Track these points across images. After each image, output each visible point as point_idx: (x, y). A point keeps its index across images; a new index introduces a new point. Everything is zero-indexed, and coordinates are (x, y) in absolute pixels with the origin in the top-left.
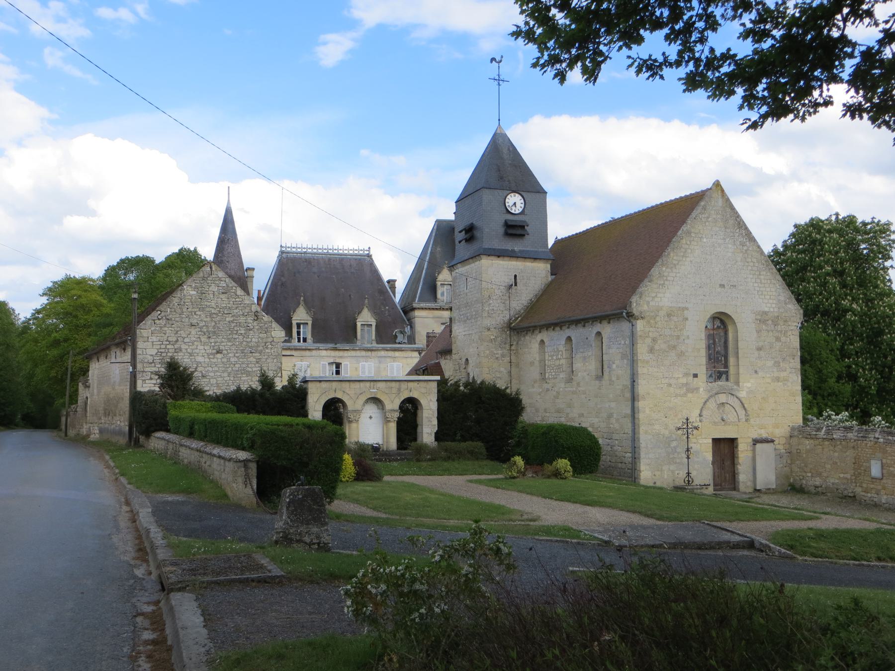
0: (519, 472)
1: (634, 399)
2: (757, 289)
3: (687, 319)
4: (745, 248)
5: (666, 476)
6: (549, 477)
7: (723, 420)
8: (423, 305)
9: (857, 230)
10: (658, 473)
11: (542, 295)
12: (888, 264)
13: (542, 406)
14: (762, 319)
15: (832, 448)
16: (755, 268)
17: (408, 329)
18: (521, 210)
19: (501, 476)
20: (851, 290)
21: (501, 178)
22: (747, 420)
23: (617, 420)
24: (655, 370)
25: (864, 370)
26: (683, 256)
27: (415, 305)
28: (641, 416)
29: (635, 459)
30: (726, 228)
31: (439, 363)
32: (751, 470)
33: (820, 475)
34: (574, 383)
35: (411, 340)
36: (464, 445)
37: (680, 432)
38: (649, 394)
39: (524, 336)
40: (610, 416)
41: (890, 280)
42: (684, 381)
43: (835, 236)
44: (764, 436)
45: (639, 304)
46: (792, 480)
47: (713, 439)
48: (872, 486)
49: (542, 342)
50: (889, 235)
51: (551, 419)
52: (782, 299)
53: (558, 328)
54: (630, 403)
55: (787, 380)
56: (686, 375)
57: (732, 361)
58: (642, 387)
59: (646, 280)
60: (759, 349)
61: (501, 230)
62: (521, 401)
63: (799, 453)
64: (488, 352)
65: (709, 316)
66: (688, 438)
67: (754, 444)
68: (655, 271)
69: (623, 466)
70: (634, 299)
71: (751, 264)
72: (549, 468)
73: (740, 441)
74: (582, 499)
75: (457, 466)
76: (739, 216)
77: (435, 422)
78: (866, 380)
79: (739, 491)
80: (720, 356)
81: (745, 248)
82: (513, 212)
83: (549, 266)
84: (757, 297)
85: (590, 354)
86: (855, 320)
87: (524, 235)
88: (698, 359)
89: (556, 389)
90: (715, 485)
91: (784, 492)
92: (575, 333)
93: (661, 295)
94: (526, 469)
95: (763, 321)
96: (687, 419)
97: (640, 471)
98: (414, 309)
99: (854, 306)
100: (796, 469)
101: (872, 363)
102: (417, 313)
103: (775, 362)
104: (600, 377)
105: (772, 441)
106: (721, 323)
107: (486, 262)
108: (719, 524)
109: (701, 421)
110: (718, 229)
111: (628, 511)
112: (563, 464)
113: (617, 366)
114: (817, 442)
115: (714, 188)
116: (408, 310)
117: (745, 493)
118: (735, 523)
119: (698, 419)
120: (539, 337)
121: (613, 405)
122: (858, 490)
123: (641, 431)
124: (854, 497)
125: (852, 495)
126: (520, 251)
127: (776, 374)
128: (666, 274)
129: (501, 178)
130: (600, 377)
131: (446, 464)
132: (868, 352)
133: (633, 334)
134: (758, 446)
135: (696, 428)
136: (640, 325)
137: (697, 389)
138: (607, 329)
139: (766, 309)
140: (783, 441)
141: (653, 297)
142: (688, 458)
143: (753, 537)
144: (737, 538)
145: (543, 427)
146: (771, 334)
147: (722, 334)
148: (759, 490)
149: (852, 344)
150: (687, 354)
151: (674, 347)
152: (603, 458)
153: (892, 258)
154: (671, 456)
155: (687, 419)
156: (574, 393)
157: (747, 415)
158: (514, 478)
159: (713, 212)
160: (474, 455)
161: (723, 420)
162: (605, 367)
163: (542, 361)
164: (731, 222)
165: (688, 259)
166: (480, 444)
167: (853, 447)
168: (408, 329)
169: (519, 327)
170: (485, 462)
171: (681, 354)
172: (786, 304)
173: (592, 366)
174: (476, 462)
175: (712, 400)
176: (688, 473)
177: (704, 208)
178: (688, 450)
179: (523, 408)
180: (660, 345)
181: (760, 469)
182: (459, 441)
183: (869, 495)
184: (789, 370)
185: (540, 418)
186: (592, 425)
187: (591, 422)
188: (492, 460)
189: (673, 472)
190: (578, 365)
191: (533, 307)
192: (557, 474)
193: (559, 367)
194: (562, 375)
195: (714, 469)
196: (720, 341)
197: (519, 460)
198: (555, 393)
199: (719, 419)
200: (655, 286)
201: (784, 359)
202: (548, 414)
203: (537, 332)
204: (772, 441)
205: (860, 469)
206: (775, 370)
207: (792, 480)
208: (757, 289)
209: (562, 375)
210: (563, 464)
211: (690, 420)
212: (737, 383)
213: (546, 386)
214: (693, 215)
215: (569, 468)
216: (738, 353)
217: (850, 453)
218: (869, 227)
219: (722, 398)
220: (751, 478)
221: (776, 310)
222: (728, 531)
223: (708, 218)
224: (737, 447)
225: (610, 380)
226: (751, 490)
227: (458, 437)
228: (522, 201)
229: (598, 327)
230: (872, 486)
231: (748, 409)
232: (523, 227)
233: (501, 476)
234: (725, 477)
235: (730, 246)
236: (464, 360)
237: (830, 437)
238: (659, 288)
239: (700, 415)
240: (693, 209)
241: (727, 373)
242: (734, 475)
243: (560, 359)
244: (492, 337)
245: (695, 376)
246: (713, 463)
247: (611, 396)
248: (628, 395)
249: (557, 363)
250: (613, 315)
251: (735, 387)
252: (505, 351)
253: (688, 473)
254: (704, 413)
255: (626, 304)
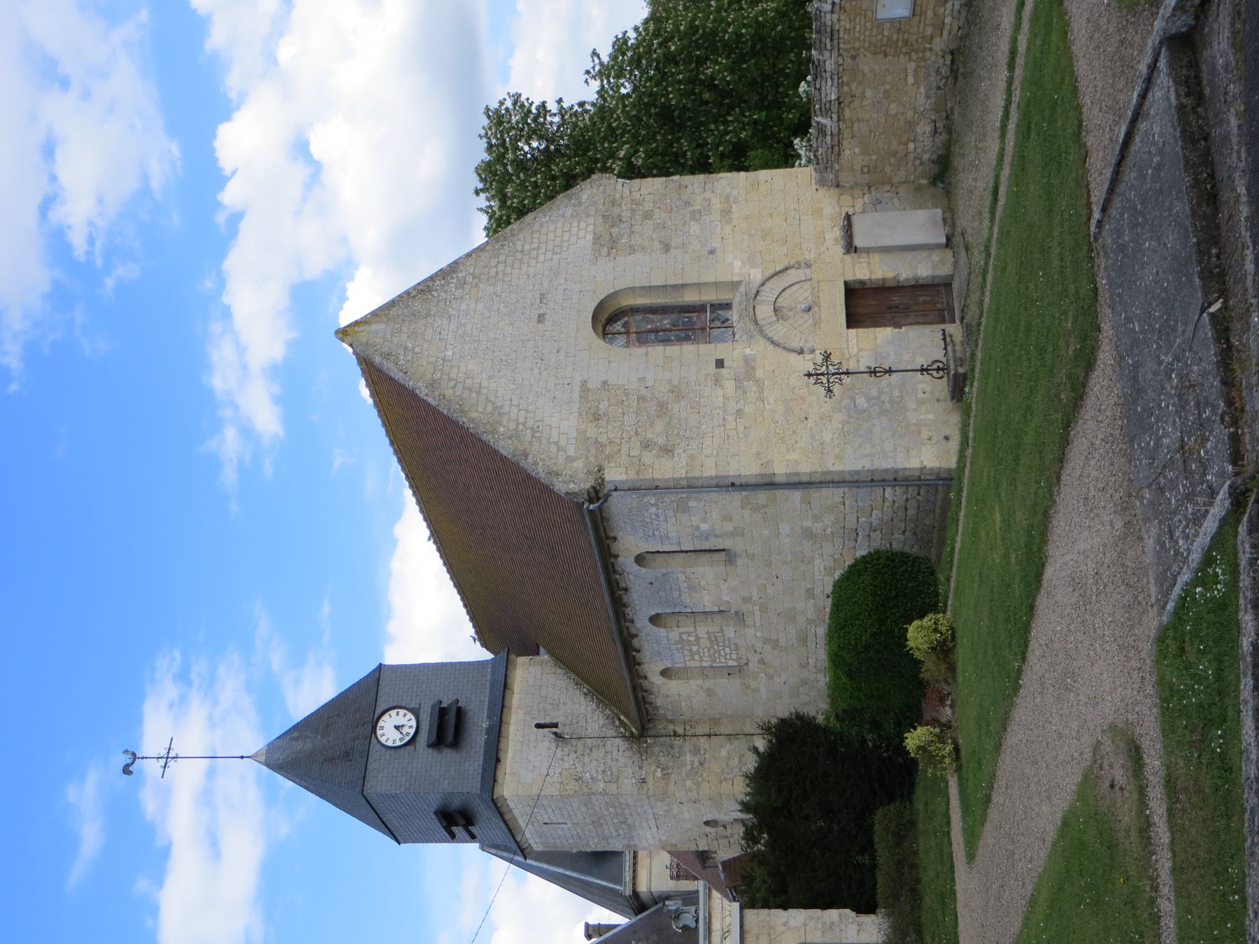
0: (941, 739)
1: (769, 484)
2: (549, 255)
3: (605, 383)
4: (469, 279)
5: (931, 417)
6: (952, 668)
7: (809, 309)
8: (628, 877)
9: (500, 158)
10: (925, 434)
11: (578, 674)
12: (552, 107)
13: (791, 672)
14: (607, 244)
15: (857, 102)
16: (510, 260)
17: (672, 905)
18: (410, 715)
19: (953, 783)
20: (597, 161)
21: (347, 755)
22: (808, 266)
23: (816, 518)
24: (708, 442)
25: (727, 133)
26: (479, 393)
27: (628, 892)
28: (806, 467)
29: (896, 479)
30: (428, 315)
31: (723, 863)
32: (909, 255)
33: (911, 125)
34: (745, 608)
35: (690, 898)
36: (882, 856)
37: (836, 388)
38: (758, 454)
39: (657, 708)
40: (809, 534)
41: (581, 104)
42: (730, 385)
43: (509, 190)
44: (838, 232)
45: (571, 476)
46: (924, 182)
47: (849, 326)
48: (930, 14)
49: (665, 673)
50: (507, 110)
51: (819, 654)
52: (569, 211)
53: (635, 642)
54: (780, 493)
55: (728, 196)
56: (718, 382)
57: (690, 298)
58: (745, 467)
59: (523, 464)
60: (667, 248)
61: (448, 754)
62: (783, 721)
63: (868, 169)
64: (688, 783)
65: (601, 342)
66: (847, 373)
67: (856, 250)
68: (506, 447)
69: (912, 504)
70: (561, 487)
71: (501, 267)
72: (931, 669)
73: (850, 277)
74: (1017, 589)
75: (931, 874)
76: (407, 293)
77: (833, 914)
78: (743, 129)
79: (952, 276)
80: (683, 319)
81: (469, 279)
82: (412, 731)
83: (521, 660)
84: (564, 255)
85: (682, 577)
86: (645, 152)
87: (459, 710)
88: (688, 359)
89: (758, 645)
90: (943, 321)
91: (948, 193)
92: (641, 607)
93: (555, 433)
94: (935, 722)
95: (613, 243)
96: (809, 375)
97: (922, 469)
98: (635, 894)
99: (622, 154)
100: (901, 175)
101: (715, 122)
102: (642, 888)
103: (693, 218)
104: (728, 556)
105: (848, 217)
106: (611, 319)
107: (510, 787)
108: (1098, 195)
109: (813, 351)
110: (429, 331)
111: (1061, 460)
112: (918, 635)
113: (704, 520)
114: (846, 134)
115: (349, 338)
116: (637, 904)
117: (956, 264)
118: (1090, 141)
119: (808, 357)
120: (656, 679)
121: (784, 528)
122: (938, 44)
123: (838, 467)
124: (952, 53)
125: (949, 57)
126: (490, 717)
127: (716, 216)
128: (512, 426)
129: (347, 755)
130: (728, 556)
131: (929, 900)
132: (698, 129)
133: (634, 489)
134: (858, 242)
135: (827, 357)
136: (614, 475)
137: (747, 360)
138: (629, 543)
139: (590, 237)
140: (846, 200)
141: (559, 450)
142: (890, 371)
143: (1152, 41)
144: (1165, 92)
145: (836, 678)
146: (637, 228)
147: (639, 317)
148: (948, 239)
149: (684, 154)
150: (675, 382)
151: (662, 406)
152: (896, 547)
153: (544, 103)
154: (888, 406)
155: (809, 375)
156: (764, 608)
157: (798, 266)
158: (957, 750)
159: (396, 340)
160: (905, 831)
161: (809, 309)
162: (706, 545)
163: (703, 672)
164: (417, 306)
165: (485, 384)
166: (879, 816)
167: (854, 57)
168: (672, 905)
169: (639, 717)
170: (919, 805)
171: (676, 392)
172: (580, 204)
173: (706, 572)
174: (920, 826)
175: (770, 331)
176: (922, 370)
177: (387, 356)
178: (873, 372)
179: (799, 717)
180: (657, 432)
181: (904, 240)
182: (873, 858)
183: (948, 20)
184: (708, 195)
185: (820, 677)
186: (829, 571)
187: (823, 571)
188: (912, 785)
189: (920, 403)
190: (707, 601)
191: (600, 692)
192: (944, 649)
193: (713, 639)
194: (730, 633)
195: (911, 324)
196: (653, 321)
197: (915, 739)
198: (768, 647)
199: (806, 316)
200: (536, 446)
201: (687, 203)
202: (811, 661)
203: (645, 684)
204: (848, 217)
205: (897, 40)
206: (707, 218)
207: (924, 182)
208: (549, 255)
209: (730, 633)
210: (918, 635)
211: (811, 369)
212: (734, 285)
213: (753, 666)
214: (398, 375)
215: (928, 621)
216: (674, 286)
217: (867, 63)
218: (494, 141)
219: (764, 311)
220: (925, 253)
221: (591, 221)
222: (1129, 136)
223: (406, 348)
224: (862, 282)
225: (733, 534)
226: (949, 254)
227: (866, 860)
228: (393, 713)
229: (626, 561)
230: (930, 14)
231: (786, 264)
232: (443, 712)
233: (953, 783)
234: (925, 303)
235: (464, 306)
236: (708, 829)
237: (835, 107)
238: (540, 439)
239: (801, 352)
240: (391, 379)
241: (716, 307)
242: (918, 287)
243: (697, 639)
244: (659, 774)
245: (720, 364)
246: (898, 325)
247: (766, 532)
248: (762, 496)
249: (704, 642)
250: (596, 529)
251: (742, 289)
252: (688, 746)
253: (922, 370)
254: (795, 344)
255: (571, 503)
